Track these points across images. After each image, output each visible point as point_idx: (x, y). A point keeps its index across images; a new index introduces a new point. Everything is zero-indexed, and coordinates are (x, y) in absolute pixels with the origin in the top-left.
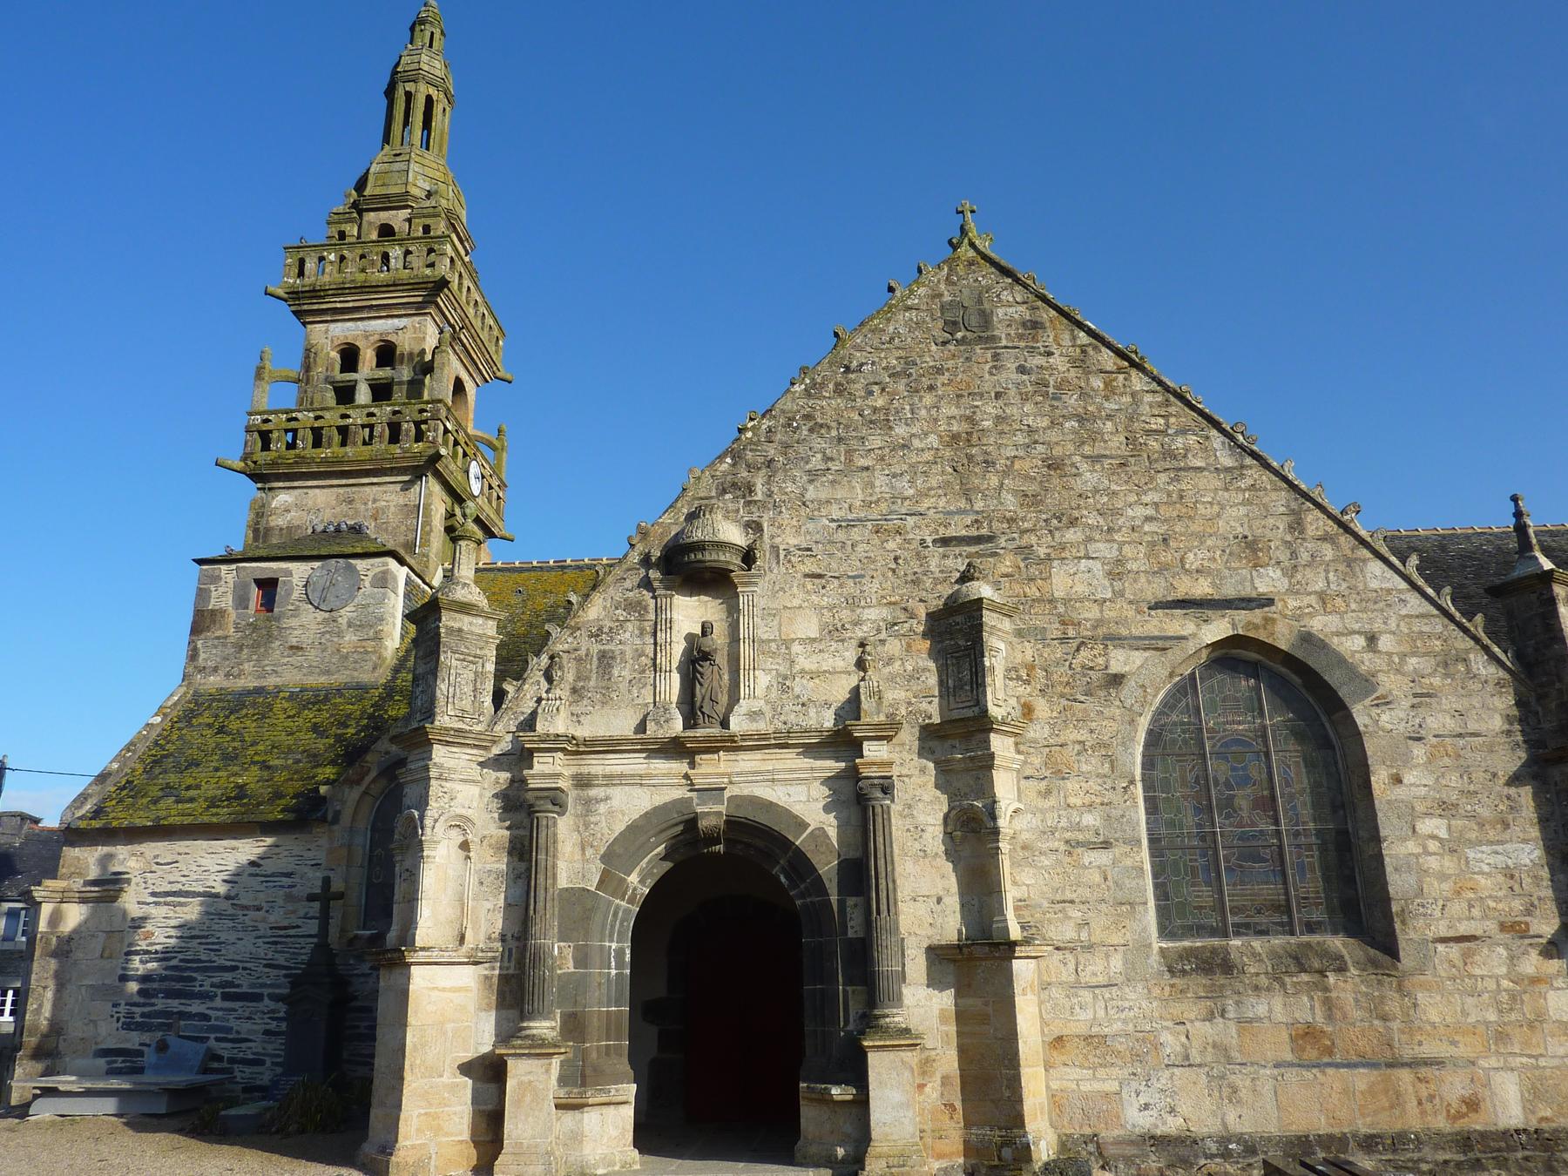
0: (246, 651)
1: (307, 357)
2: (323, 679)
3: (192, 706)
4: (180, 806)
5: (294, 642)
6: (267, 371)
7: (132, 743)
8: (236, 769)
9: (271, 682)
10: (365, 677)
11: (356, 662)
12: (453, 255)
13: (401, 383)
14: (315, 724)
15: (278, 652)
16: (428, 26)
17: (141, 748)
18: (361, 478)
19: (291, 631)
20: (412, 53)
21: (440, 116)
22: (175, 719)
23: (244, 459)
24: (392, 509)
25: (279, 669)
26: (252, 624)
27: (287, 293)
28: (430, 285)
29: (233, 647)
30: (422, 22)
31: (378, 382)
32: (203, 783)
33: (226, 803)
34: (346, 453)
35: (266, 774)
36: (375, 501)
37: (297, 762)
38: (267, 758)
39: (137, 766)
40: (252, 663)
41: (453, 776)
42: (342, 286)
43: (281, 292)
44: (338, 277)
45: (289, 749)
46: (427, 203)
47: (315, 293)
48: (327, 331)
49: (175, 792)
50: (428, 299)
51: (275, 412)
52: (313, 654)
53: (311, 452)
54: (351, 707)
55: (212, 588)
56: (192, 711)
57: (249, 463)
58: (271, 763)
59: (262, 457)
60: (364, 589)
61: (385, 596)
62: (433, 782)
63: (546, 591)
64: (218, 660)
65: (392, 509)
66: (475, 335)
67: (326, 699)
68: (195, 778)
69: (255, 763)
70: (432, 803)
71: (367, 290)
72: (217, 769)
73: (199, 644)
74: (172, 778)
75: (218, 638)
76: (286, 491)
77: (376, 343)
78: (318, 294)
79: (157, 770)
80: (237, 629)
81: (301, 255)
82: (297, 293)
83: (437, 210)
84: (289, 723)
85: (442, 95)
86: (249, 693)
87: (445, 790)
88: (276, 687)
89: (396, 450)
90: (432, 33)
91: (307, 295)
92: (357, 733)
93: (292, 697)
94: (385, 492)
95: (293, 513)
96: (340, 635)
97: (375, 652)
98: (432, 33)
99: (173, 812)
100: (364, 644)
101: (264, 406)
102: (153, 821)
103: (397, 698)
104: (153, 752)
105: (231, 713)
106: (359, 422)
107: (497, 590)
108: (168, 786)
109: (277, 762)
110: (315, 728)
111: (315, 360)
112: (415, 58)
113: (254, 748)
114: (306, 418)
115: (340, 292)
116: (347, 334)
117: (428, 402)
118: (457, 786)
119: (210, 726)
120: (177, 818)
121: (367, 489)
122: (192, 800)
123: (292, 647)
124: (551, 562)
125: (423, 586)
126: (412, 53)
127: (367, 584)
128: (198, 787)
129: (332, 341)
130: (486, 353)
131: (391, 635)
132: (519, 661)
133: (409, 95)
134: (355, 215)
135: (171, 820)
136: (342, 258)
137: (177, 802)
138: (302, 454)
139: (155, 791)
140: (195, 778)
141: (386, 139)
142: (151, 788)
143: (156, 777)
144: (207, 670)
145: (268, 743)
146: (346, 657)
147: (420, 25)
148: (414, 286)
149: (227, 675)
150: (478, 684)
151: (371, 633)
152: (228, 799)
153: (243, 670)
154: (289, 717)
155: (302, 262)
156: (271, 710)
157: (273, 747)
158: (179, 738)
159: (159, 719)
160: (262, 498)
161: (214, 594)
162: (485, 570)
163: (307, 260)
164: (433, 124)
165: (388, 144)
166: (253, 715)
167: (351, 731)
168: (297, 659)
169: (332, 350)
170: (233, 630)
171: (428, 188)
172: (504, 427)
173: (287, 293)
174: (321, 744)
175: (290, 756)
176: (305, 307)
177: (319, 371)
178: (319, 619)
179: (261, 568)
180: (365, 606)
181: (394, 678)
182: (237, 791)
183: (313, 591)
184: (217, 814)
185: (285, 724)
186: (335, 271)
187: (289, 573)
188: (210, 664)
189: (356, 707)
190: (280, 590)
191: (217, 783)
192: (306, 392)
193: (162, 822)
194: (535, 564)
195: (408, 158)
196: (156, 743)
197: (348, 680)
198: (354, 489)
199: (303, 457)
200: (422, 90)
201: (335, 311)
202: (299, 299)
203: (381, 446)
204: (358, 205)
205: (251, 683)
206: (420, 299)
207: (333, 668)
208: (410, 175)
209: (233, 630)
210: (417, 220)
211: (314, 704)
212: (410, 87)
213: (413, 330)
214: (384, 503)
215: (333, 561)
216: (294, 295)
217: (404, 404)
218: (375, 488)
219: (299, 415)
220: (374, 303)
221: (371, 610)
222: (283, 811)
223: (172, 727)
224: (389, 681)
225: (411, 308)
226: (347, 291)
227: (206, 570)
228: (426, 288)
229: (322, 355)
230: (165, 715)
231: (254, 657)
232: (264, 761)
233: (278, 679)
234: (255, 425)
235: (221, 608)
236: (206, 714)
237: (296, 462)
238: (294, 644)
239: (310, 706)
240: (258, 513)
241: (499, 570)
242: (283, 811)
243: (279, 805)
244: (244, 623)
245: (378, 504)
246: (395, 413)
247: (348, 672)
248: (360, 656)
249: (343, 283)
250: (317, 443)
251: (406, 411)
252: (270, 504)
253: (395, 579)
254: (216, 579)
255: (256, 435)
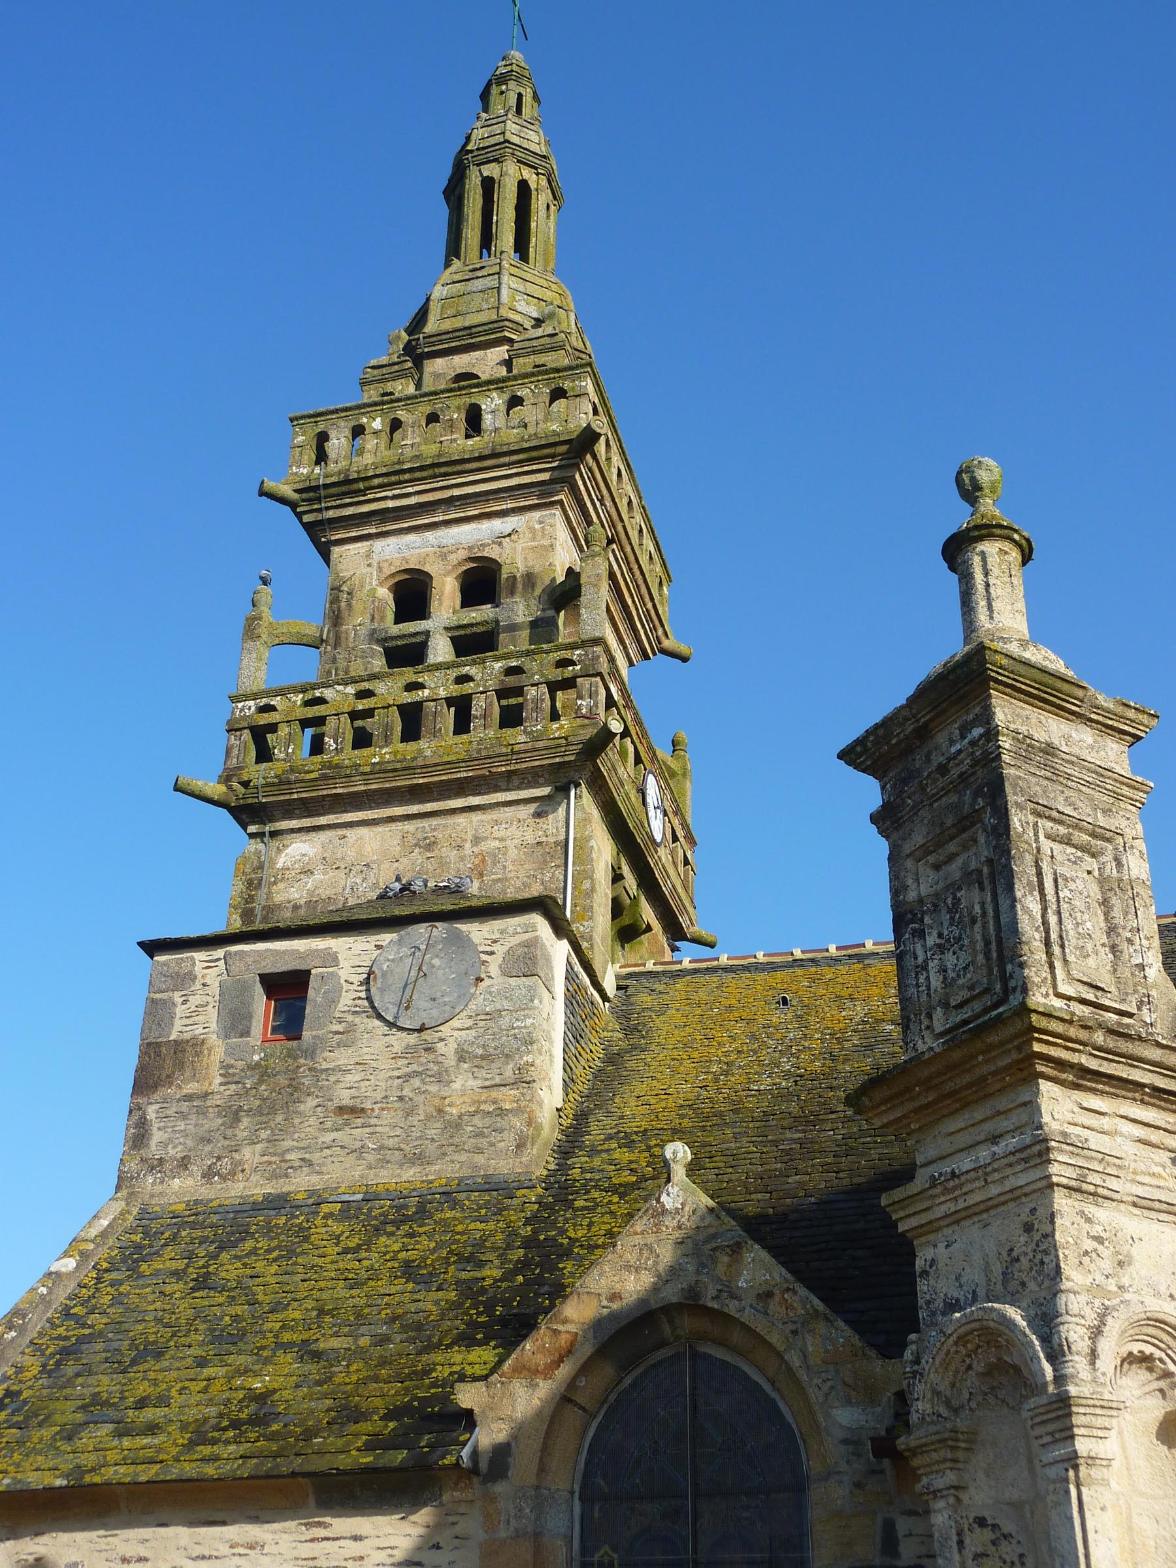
0: (245, 1122)
1: (335, 600)
2: (410, 1174)
3: (137, 1238)
4: (126, 1442)
5: (345, 1097)
6: (264, 623)
7: (17, 1312)
8: (242, 1360)
9: (300, 1183)
10: (503, 1166)
11: (479, 1134)
12: (597, 401)
13: (513, 628)
14: (407, 1263)
15: (312, 1121)
16: (512, 85)
17: (36, 1323)
18: (449, 798)
19: (339, 1075)
20: (489, 122)
21: (542, 212)
22: (105, 1265)
23: (226, 779)
24: (513, 853)
25: (316, 1157)
26: (258, 1065)
27: (295, 491)
28: (564, 448)
29: (219, 1115)
30: (502, 79)
31: (468, 631)
32: (174, 1392)
33: (230, 1433)
34: (420, 751)
35: (313, 1369)
36: (477, 840)
37: (383, 1340)
38: (313, 1335)
39: (28, 1360)
40: (259, 1147)
41: (1113, 1183)
42: (397, 467)
43: (287, 490)
44: (388, 455)
45: (358, 1316)
46: (539, 332)
47: (349, 486)
48: (369, 554)
49: (112, 1413)
50: (557, 474)
51: (282, 692)
52: (387, 1124)
53: (350, 756)
54: (481, 1226)
55: (177, 997)
56: (138, 1247)
57: (235, 785)
58: (322, 1345)
59: (258, 773)
60: (487, 982)
61: (532, 995)
62: (1062, 1202)
63: (840, 997)
64: (190, 1143)
65: (513, 853)
66: (632, 558)
67: (423, 1212)
68: (155, 1382)
69: (286, 1346)
70: (1074, 1276)
71: (443, 470)
72: (202, 1363)
73: (151, 1112)
74: (106, 1384)
75: (189, 1098)
76: (304, 836)
77: (459, 564)
78: (355, 486)
79: (70, 1369)
80: (228, 1076)
81: (321, 427)
82: (316, 488)
83: (556, 338)
84: (348, 1262)
85: (544, 182)
86: (256, 1207)
87: (1097, 1230)
88: (311, 1193)
89: (517, 736)
90: (520, 96)
91: (334, 490)
92: (508, 1276)
93: (348, 1211)
94: (497, 822)
95: (318, 876)
96: (442, 1078)
97: (518, 1111)
98: (520, 96)
99: (112, 1456)
100: (494, 1094)
101: (260, 683)
102: (67, 1476)
103: (579, 1203)
104: (61, 1331)
105: (221, 1248)
106: (442, 693)
107: (734, 1002)
108: (96, 1400)
109: (335, 1343)
110: (409, 1270)
111: (349, 605)
112: (497, 129)
113: (280, 1316)
114: (340, 696)
115: (393, 478)
116: (407, 554)
117: (574, 646)
118: (1130, 1223)
119: (178, 1275)
120: (122, 1470)
121: (461, 820)
122: (152, 1429)
123: (341, 1110)
124: (832, 949)
125: (592, 990)
126: (489, 122)
127: (494, 969)
128: (163, 1401)
129: (380, 569)
130: (647, 599)
131: (546, 1078)
132: (834, 1121)
133: (488, 185)
134: (410, 364)
135: (108, 1474)
136: (396, 425)
137: (120, 1434)
138: (336, 760)
139: (67, 1412)
140: (155, 1382)
141: (454, 249)
142: (59, 1405)
143: (70, 1383)
144: (167, 1166)
145: (310, 1304)
146: (456, 1125)
147: (499, 84)
148: (532, 453)
149: (208, 1174)
150: (1117, 912)
151: (509, 1072)
152: (235, 1424)
153: (240, 1163)
154: (346, 1251)
155: (323, 438)
156: (306, 1239)
157: (322, 1312)
158: (117, 1301)
159: (70, 1264)
160: (258, 853)
161: (180, 1010)
162: (697, 971)
163: (333, 434)
164: (533, 225)
165: (458, 258)
166: (268, 1251)
167: (492, 1272)
168: (351, 1135)
169: (381, 584)
170: (219, 1080)
171: (535, 315)
172: (683, 735)
173: (295, 491)
174: (430, 1303)
175: (363, 1329)
176: (331, 514)
177: (358, 623)
178: (398, 1048)
179: (276, 953)
180: (490, 1016)
181: (563, 1168)
182: (253, 1407)
183: (382, 991)
184: (215, 1458)
185: (341, 1265)
186: (383, 446)
187: (332, 959)
188: (172, 1152)
189: (491, 1226)
190: (314, 994)
191: (205, 1390)
192: (334, 660)
193: (88, 1479)
194: (798, 954)
195: (496, 269)
196: (66, 1313)
197: (465, 1172)
198: (435, 821)
199: (337, 766)
200: (511, 172)
201: (384, 515)
202: (319, 500)
203: (484, 733)
204: (415, 348)
205: (257, 1188)
206: (545, 476)
207: (431, 1148)
208: (505, 292)
209: (219, 1080)
210: (521, 360)
211: (398, 1224)
212: (490, 170)
213: (528, 535)
214: (497, 844)
215: (422, 929)
216: (312, 492)
217: (528, 653)
218: (476, 817)
219: (328, 693)
220: (456, 492)
221: (504, 1022)
222: (369, 1447)
223: (99, 1280)
224: (552, 1174)
225: (525, 497)
226: (407, 476)
227: (164, 964)
228: (553, 456)
229: (361, 595)
230: (84, 1256)
231: (264, 1134)
232: (305, 1342)
233: (315, 1178)
234: (245, 717)
235: (195, 1038)
236: (169, 1252)
237: (324, 777)
238: (347, 1102)
239: (390, 1228)
240: (250, 883)
241: (726, 969)
242: (369, 1447)
243: (357, 1435)
244: (240, 1064)
245: (483, 847)
246: (510, 671)
247: (463, 1157)
248: (487, 1121)
249: (399, 462)
250: (362, 740)
251: (531, 665)
252: (273, 862)
253: (548, 960)
254: (184, 980)
255: (246, 735)
